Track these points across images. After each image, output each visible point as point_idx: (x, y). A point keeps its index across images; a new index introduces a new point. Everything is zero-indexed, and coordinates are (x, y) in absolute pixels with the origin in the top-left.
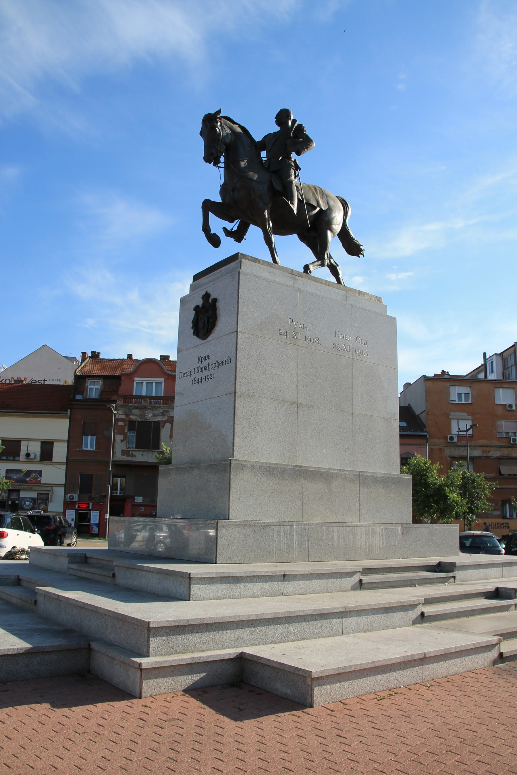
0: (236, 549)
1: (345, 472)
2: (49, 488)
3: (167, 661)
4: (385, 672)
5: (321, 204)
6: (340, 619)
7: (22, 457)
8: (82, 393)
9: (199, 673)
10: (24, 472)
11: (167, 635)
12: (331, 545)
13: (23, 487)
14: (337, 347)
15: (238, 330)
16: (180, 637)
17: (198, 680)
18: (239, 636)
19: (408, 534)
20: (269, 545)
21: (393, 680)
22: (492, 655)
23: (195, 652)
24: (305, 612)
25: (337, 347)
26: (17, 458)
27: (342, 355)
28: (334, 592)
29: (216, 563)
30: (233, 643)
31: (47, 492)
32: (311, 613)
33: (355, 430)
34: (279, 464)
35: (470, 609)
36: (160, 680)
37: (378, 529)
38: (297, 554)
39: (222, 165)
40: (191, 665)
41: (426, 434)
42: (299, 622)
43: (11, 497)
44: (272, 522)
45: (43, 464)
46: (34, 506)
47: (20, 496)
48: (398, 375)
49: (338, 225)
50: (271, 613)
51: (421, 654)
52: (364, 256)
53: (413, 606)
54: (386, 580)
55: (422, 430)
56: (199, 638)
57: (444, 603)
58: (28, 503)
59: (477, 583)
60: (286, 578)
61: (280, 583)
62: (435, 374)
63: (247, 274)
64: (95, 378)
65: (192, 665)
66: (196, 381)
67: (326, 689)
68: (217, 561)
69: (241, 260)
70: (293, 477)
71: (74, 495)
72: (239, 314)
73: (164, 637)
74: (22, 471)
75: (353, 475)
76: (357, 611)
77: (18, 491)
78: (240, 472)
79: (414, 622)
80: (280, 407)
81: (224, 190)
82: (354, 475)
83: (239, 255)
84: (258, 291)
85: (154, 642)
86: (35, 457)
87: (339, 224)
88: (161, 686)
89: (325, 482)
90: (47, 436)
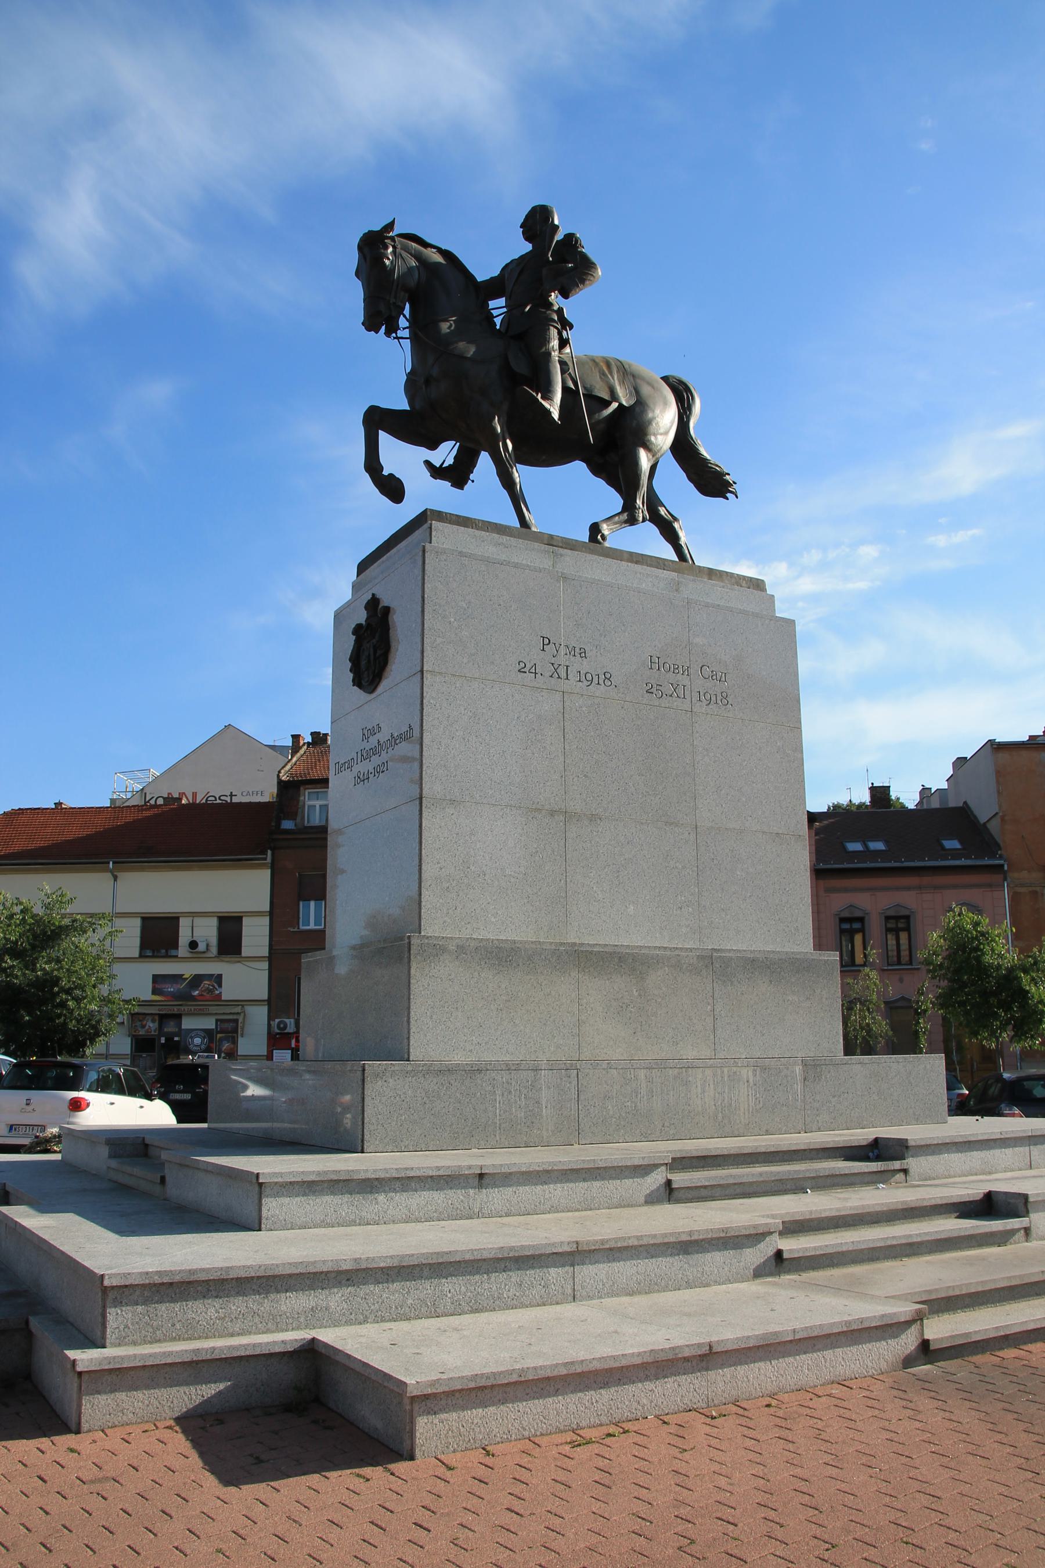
0: (408, 1122)
1: (677, 952)
2: (238, 1009)
3: (135, 1355)
4: (606, 1385)
5: (620, 395)
6: (567, 1268)
7: (183, 950)
8: (292, 816)
9: (215, 1383)
10: (187, 978)
11: (145, 1302)
12: (631, 1107)
13: (186, 1008)
14: (654, 690)
15: (425, 669)
16: (177, 1306)
17: (212, 1397)
18: (317, 1305)
19: (819, 1080)
20: (485, 1111)
21: (627, 1403)
22: (901, 1346)
23: (211, 1337)
24: (475, 1253)
25: (654, 690)
26: (173, 952)
27: (667, 706)
28: (603, 1209)
29: (362, 1152)
30: (302, 1319)
31: (235, 1017)
32: (491, 1256)
33: (703, 863)
34: (521, 942)
35: (904, 1241)
36: (122, 1396)
37: (744, 1071)
38: (550, 1129)
39: (406, 333)
40: (194, 1365)
41: (1002, 862)
42: (465, 1275)
43: (166, 1030)
44: (491, 1064)
45: (223, 961)
46: (211, 1045)
47: (183, 1027)
48: (802, 741)
49: (661, 434)
50: (391, 1257)
51: (699, 1345)
52: (737, 497)
53: (756, 1237)
54: (731, 1181)
55: (993, 856)
56: (221, 1308)
57: (852, 1228)
58: (197, 1041)
59: (954, 1183)
60: (485, 1181)
61: (471, 1191)
62: (1030, 736)
63: (441, 553)
64: (319, 786)
65: (197, 1364)
66: (362, 779)
67: (447, 1420)
68: (365, 1147)
69: (431, 524)
70: (555, 967)
71: (287, 1021)
72: (425, 636)
73: (138, 1306)
74: (184, 977)
75: (698, 958)
76: (611, 1249)
77: (178, 1017)
78: (431, 962)
79: (758, 1273)
80: (524, 823)
81: (412, 386)
82: (701, 958)
83: (429, 513)
84: (467, 584)
85: (116, 1318)
86: (207, 949)
87: (666, 433)
88: (125, 1409)
89: (629, 975)
90: (230, 906)
